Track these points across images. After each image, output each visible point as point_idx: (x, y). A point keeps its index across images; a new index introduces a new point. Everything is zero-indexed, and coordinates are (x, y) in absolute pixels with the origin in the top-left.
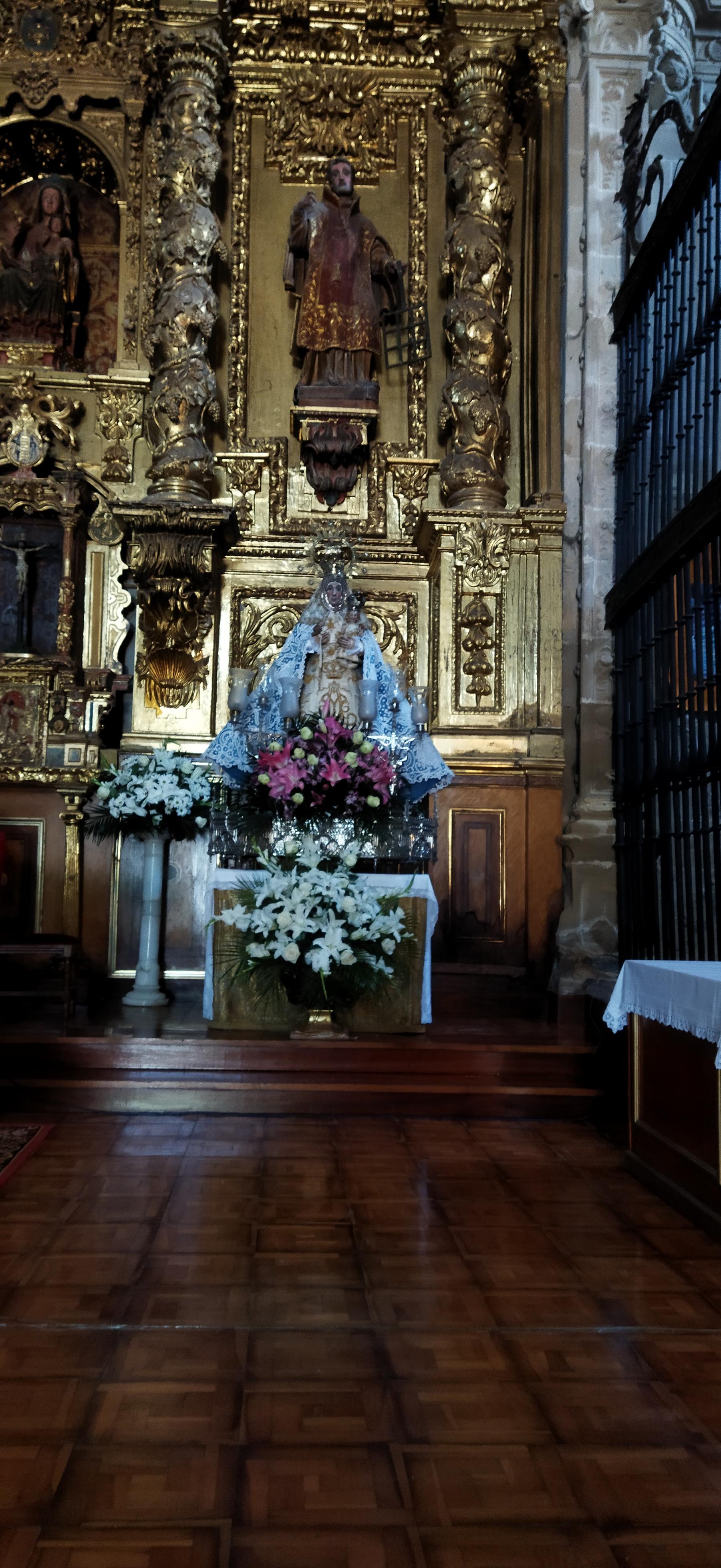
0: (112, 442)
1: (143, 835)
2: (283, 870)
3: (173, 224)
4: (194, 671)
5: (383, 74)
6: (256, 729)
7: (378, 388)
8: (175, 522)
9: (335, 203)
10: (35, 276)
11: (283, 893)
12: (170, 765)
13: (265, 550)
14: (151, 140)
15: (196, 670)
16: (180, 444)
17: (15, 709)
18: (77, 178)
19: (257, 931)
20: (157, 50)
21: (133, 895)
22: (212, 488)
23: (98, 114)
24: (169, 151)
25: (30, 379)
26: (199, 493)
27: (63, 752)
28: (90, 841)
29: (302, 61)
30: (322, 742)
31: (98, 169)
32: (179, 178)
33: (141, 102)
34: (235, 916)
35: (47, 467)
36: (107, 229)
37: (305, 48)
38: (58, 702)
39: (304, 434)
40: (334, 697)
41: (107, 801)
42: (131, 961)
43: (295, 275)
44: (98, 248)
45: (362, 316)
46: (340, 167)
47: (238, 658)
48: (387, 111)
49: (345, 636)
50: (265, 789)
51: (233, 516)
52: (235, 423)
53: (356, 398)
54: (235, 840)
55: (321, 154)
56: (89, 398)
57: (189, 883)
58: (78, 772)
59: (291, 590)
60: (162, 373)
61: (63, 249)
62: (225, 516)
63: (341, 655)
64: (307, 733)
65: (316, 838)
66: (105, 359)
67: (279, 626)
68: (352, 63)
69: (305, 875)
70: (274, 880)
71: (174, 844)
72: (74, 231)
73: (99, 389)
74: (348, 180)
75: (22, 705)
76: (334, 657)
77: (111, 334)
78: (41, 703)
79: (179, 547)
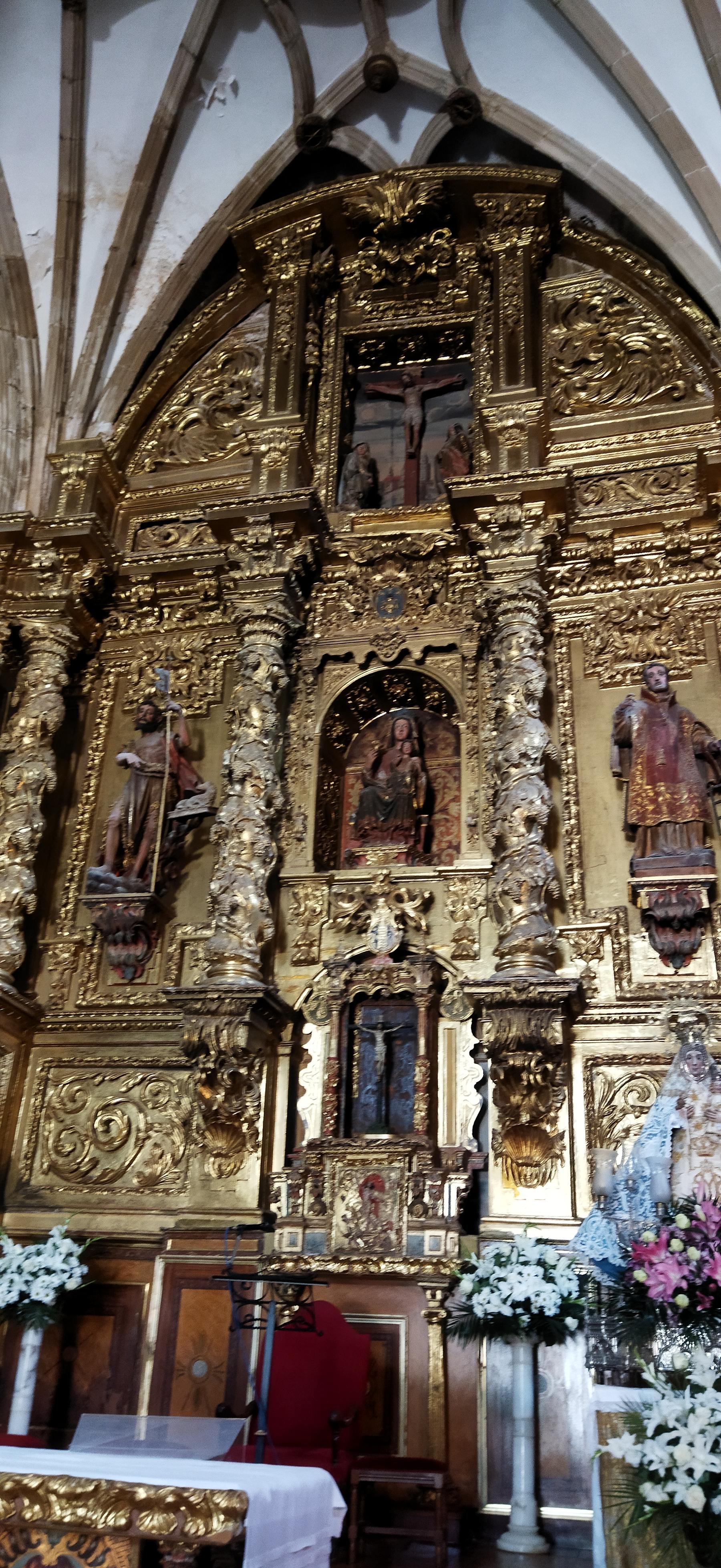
0: (459, 924)
1: (510, 1338)
2: (673, 1389)
3: (508, 737)
4: (548, 1145)
5: (685, 589)
6: (626, 1216)
7: (713, 854)
8: (524, 997)
9: (652, 699)
10: (390, 790)
11: (677, 1420)
12: (533, 1254)
13: (614, 1017)
14: (484, 671)
15: (553, 1147)
16: (523, 922)
17: (376, 1194)
18: (422, 708)
19: (652, 1468)
20: (487, 602)
21: (502, 1411)
22: (556, 960)
23: (440, 658)
24: (500, 679)
25: (387, 876)
26: (545, 966)
27: (422, 1240)
28: (454, 1344)
29: (611, 590)
30: (701, 1232)
31: (440, 699)
32: (510, 699)
33: (475, 644)
34: (623, 1447)
35: (401, 953)
36: (448, 745)
37: (613, 580)
38: (416, 1185)
39: (644, 902)
40: (708, 1177)
41: (470, 1297)
42: (504, 1493)
43: (621, 763)
44: (441, 761)
45: (690, 791)
46: (654, 670)
47: (597, 1135)
48: (693, 618)
49: (712, 1108)
50: (642, 1288)
51: (580, 987)
52: (573, 897)
53: (693, 864)
54: (615, 1350)
55: (636, 661)
56: (436, 887)
57: (562, 1398)
58: (439, 1263)
59: (644, 1056)
60: (503, 860)
61: (413, 766)
62: (573, 988)
63: (710, 1129)
64: (682, 1221)
65: (708, 1349)
66: (450, 851)
67: (634, 1095)
68: (656, 585)
69: (699, 1396)
70: (664, 1403)
71: (542, 1349)
72: (420, 751)
73: (446, 878)
74: (663, 679)
75: (382, 1189)
76: (701, 1132)
77: (454, 829)
78: (401, 1186)
79: (529, 1020)
